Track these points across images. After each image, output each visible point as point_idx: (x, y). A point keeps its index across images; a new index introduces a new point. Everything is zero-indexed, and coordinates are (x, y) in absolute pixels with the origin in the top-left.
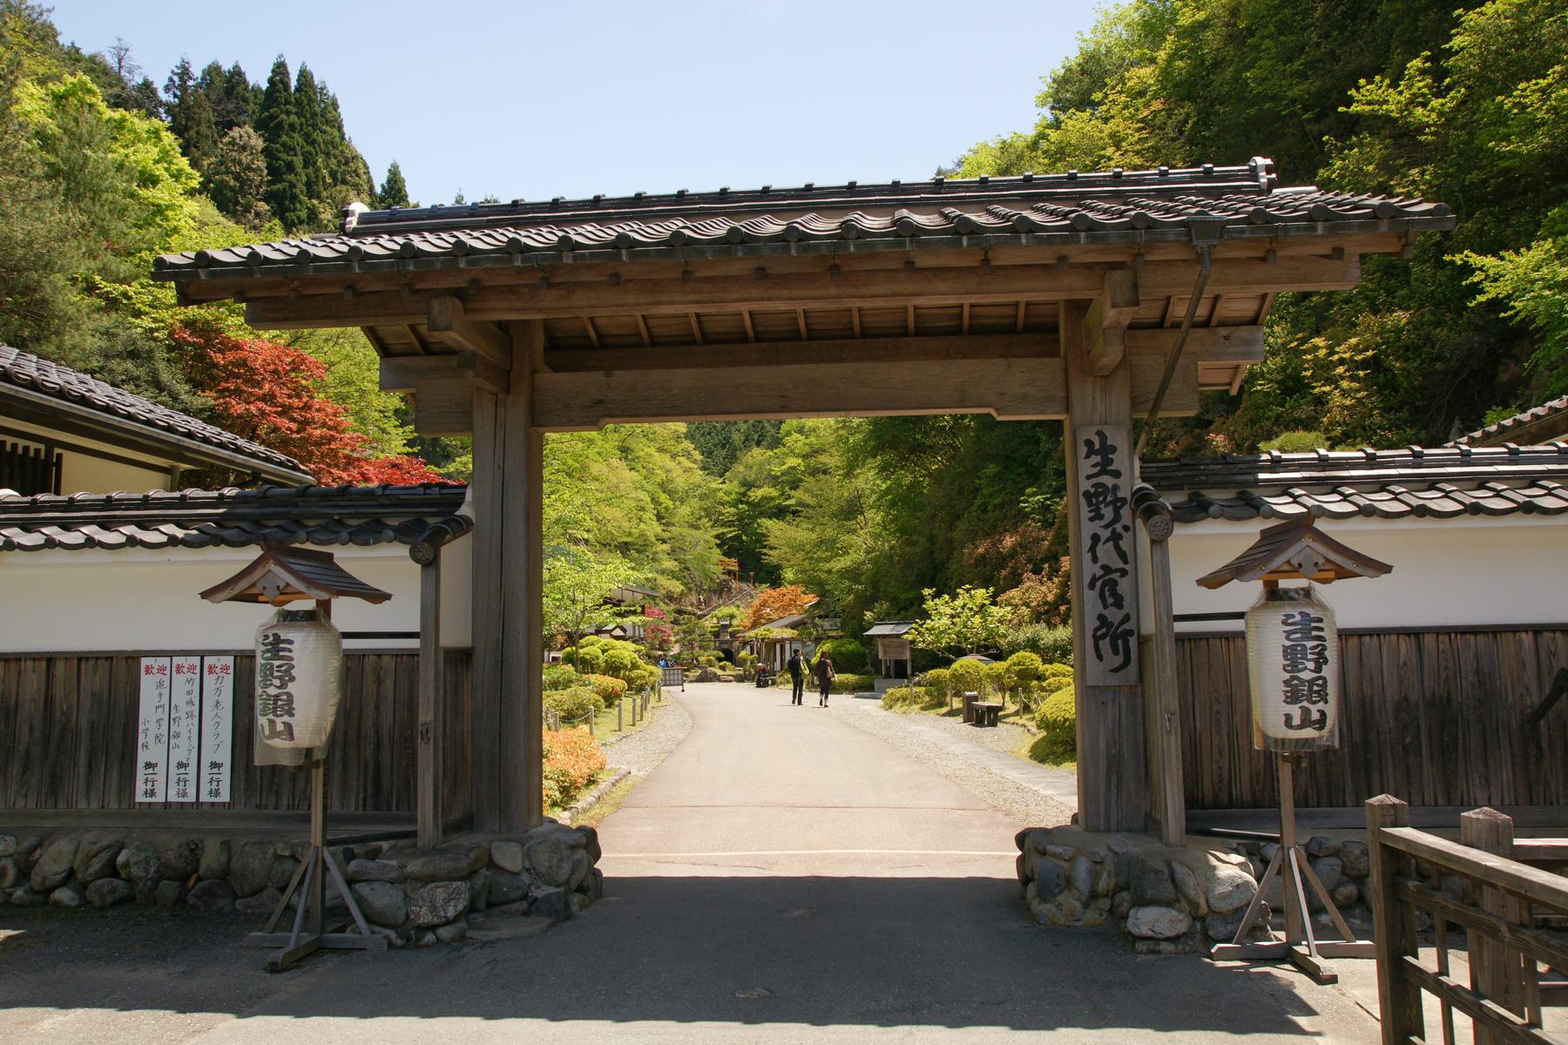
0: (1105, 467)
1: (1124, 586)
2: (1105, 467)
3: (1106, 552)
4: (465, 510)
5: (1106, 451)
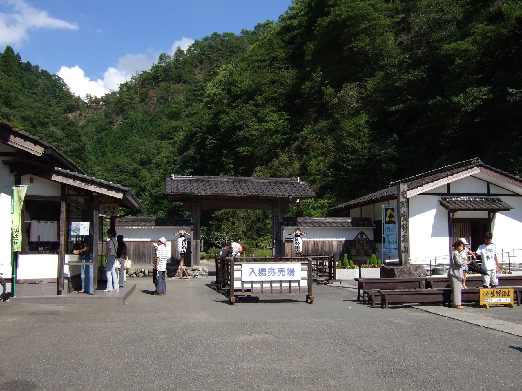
0: (277, 219)
1: (279, 234)
2: (277, 219)
3: (277, 230)
4: (192, 221)
5: (277, 216)
